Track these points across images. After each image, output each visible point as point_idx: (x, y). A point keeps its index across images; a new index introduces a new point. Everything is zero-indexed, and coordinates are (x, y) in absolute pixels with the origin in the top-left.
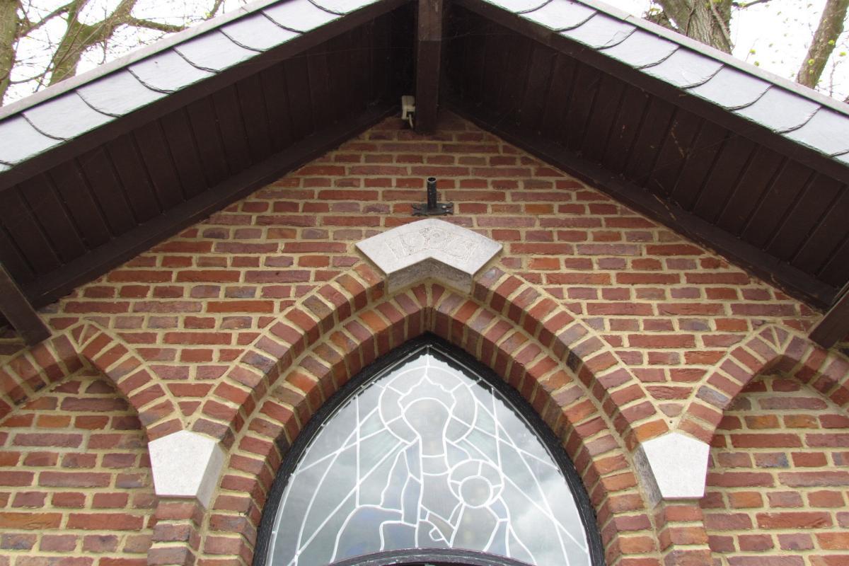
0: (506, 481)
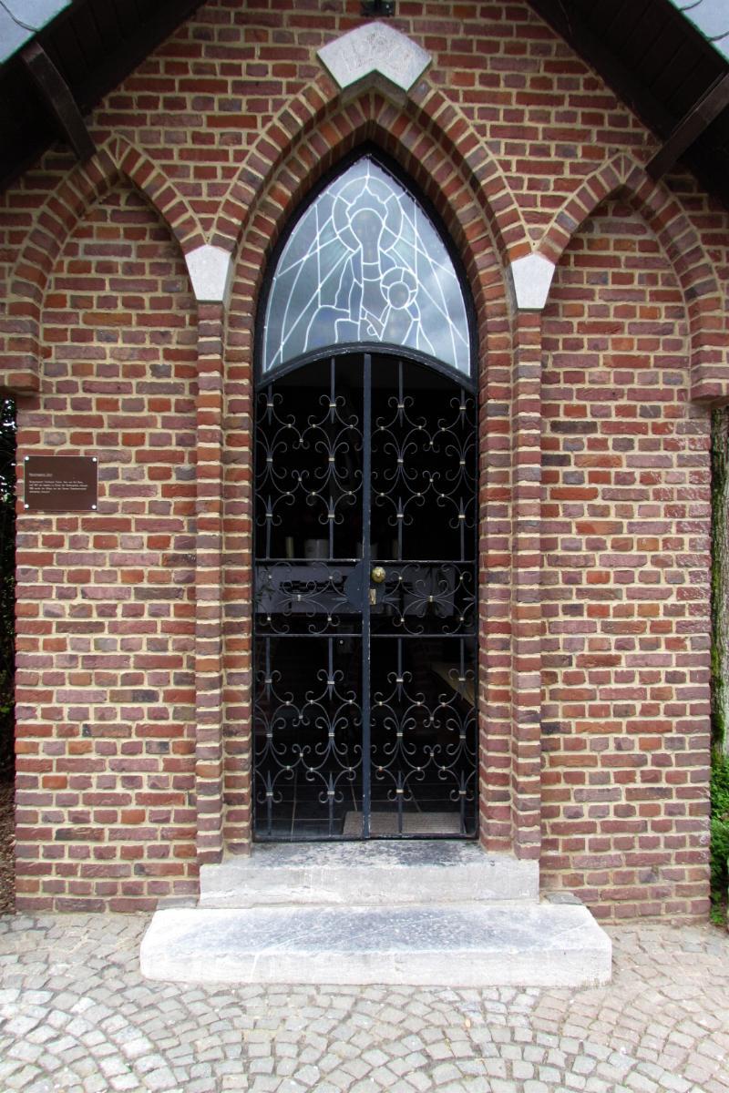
0: (420, 288)
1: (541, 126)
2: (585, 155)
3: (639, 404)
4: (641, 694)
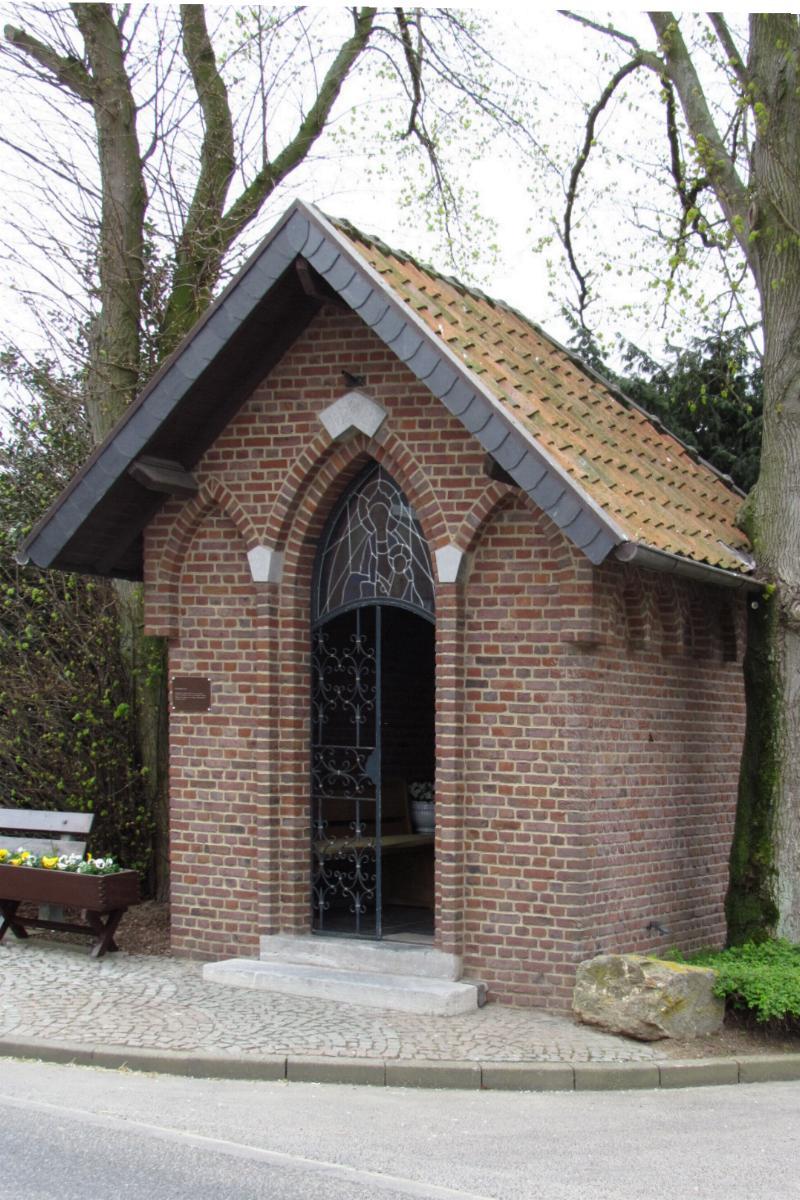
1: (456, 453)
3: (534, 644)
4: (533, 851)
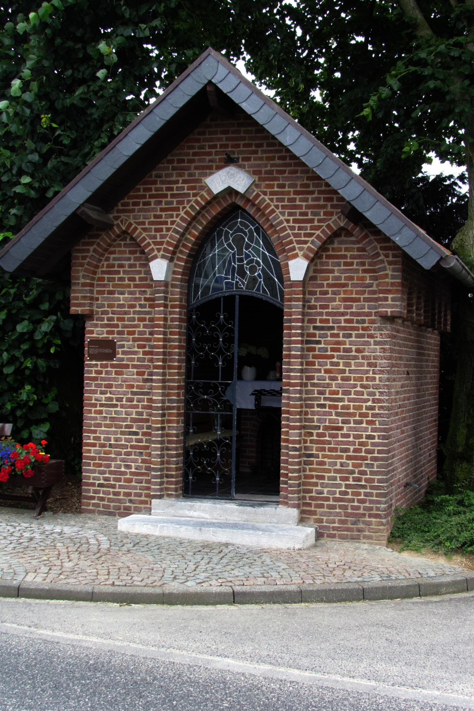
1: (304, 204)
2: (324, 215)
3: (355, 318)
4: (354, 444)
